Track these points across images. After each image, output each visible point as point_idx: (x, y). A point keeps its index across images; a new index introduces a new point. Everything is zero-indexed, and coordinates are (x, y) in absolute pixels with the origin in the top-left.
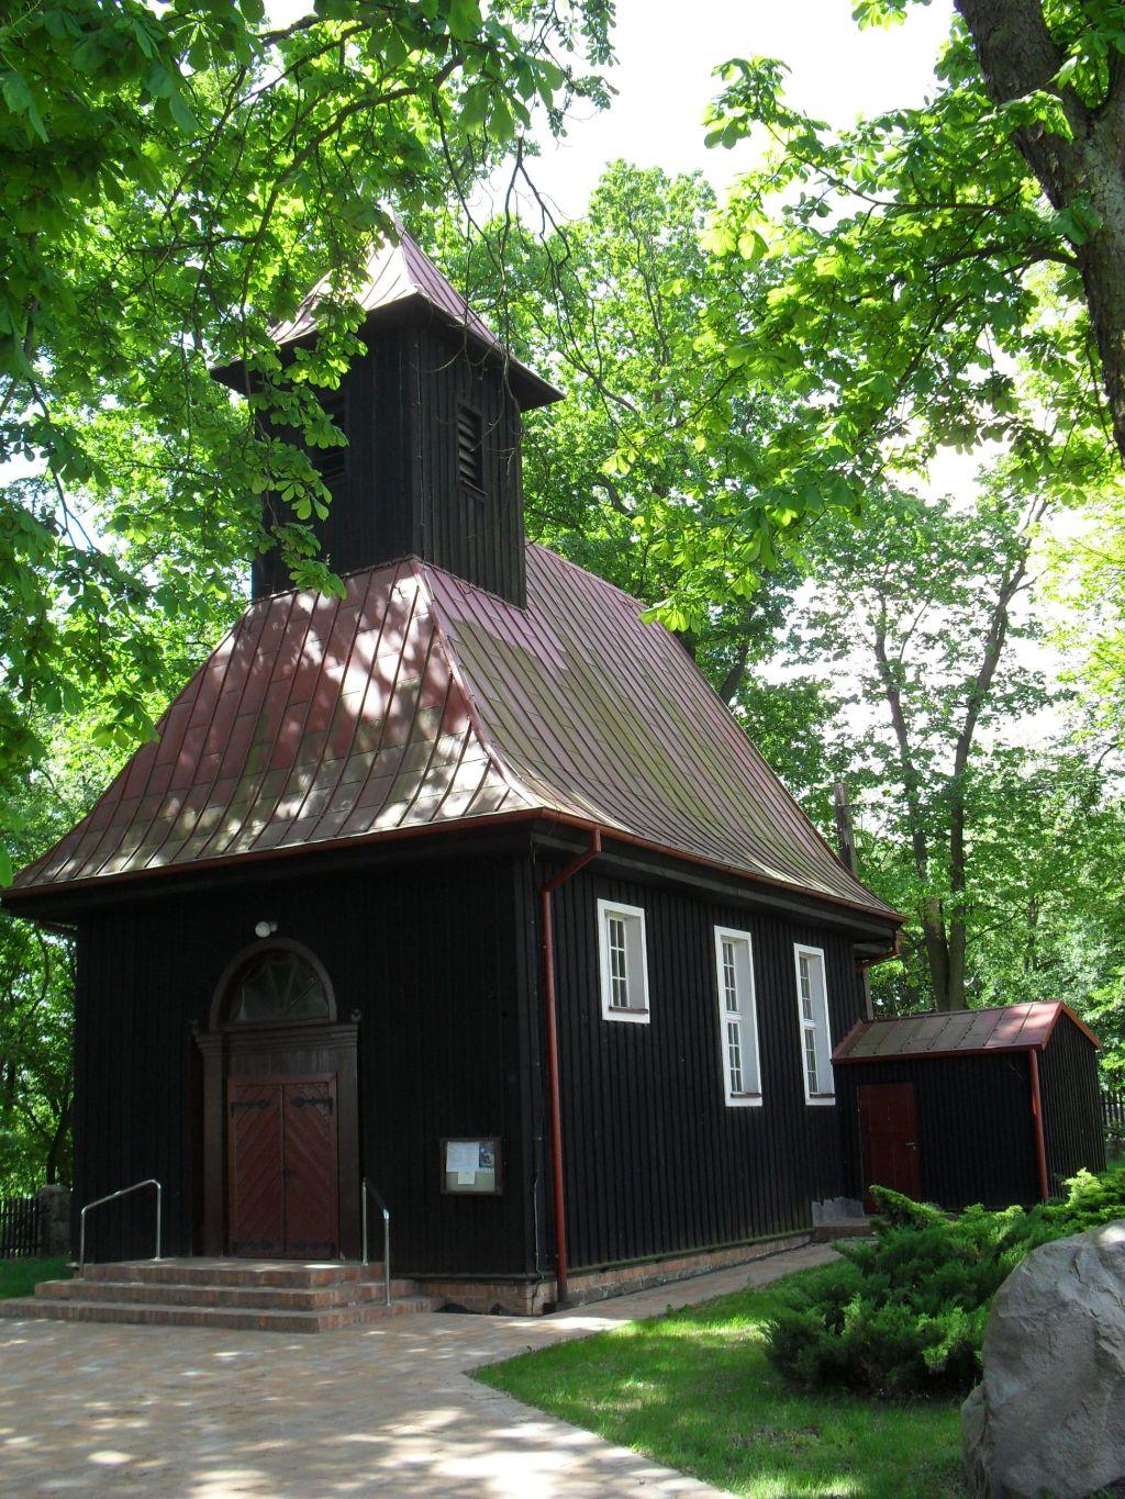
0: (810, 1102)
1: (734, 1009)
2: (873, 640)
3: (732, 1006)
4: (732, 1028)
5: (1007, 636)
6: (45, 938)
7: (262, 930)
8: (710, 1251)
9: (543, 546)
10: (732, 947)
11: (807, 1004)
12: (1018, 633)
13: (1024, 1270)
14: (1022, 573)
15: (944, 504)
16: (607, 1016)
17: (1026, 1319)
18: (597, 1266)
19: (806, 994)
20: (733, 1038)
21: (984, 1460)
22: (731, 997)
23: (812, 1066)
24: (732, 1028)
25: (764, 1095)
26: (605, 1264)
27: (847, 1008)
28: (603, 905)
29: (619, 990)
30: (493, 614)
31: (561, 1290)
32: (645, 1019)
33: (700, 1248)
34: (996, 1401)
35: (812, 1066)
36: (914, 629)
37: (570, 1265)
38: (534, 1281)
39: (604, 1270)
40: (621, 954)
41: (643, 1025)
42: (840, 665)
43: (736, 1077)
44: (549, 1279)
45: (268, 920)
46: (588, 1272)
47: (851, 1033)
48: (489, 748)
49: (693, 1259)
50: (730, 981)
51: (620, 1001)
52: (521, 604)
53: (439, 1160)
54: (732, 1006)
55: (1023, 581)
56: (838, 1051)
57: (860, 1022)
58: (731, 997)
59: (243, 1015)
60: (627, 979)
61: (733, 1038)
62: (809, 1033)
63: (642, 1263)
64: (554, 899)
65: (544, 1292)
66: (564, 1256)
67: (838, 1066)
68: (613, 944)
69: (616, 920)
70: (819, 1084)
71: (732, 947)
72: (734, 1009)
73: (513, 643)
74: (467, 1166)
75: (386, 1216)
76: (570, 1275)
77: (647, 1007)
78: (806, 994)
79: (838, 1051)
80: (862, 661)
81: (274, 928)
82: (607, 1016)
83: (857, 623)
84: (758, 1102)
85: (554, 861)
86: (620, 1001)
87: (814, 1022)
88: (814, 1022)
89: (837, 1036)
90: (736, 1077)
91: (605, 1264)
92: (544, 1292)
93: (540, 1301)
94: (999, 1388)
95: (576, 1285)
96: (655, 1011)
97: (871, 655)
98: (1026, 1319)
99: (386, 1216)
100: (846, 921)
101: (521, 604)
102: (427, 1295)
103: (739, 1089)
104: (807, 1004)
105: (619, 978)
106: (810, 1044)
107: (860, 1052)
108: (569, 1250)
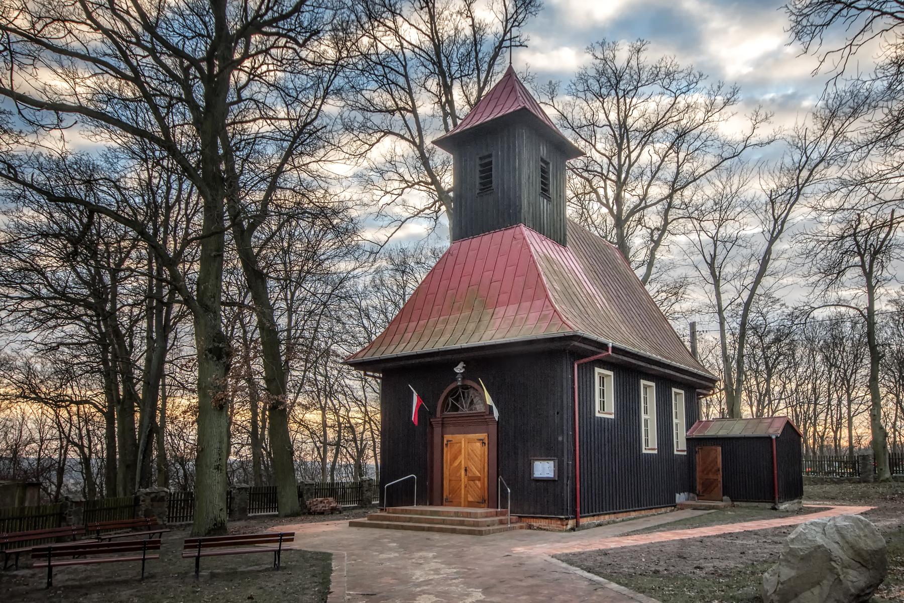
6: (230, 121)
10: (648, 392)
16: (597, 415)
24: (646, 421)
27: (692, 416)
30: (552, 248)
31: (577, 523)
44: (572, 518)
47: (694, 426)
52: (564, 246)
54: (646, 413)
63: (609, 514)
67: (688, 440)
69: (493, 159)
70: (680, 446)
71: (648, 392)
74: (544, 469)
76: (581, 517)
82: (597, 415)
85: (577, 355)
87: (679, 421)
88: (679, 421)
92: (571, 523)
93: (569, 527)
95: (584, 521)
96: (616, 413)
100: (695, 380)
101: (564, 246)
107: (696, 434)
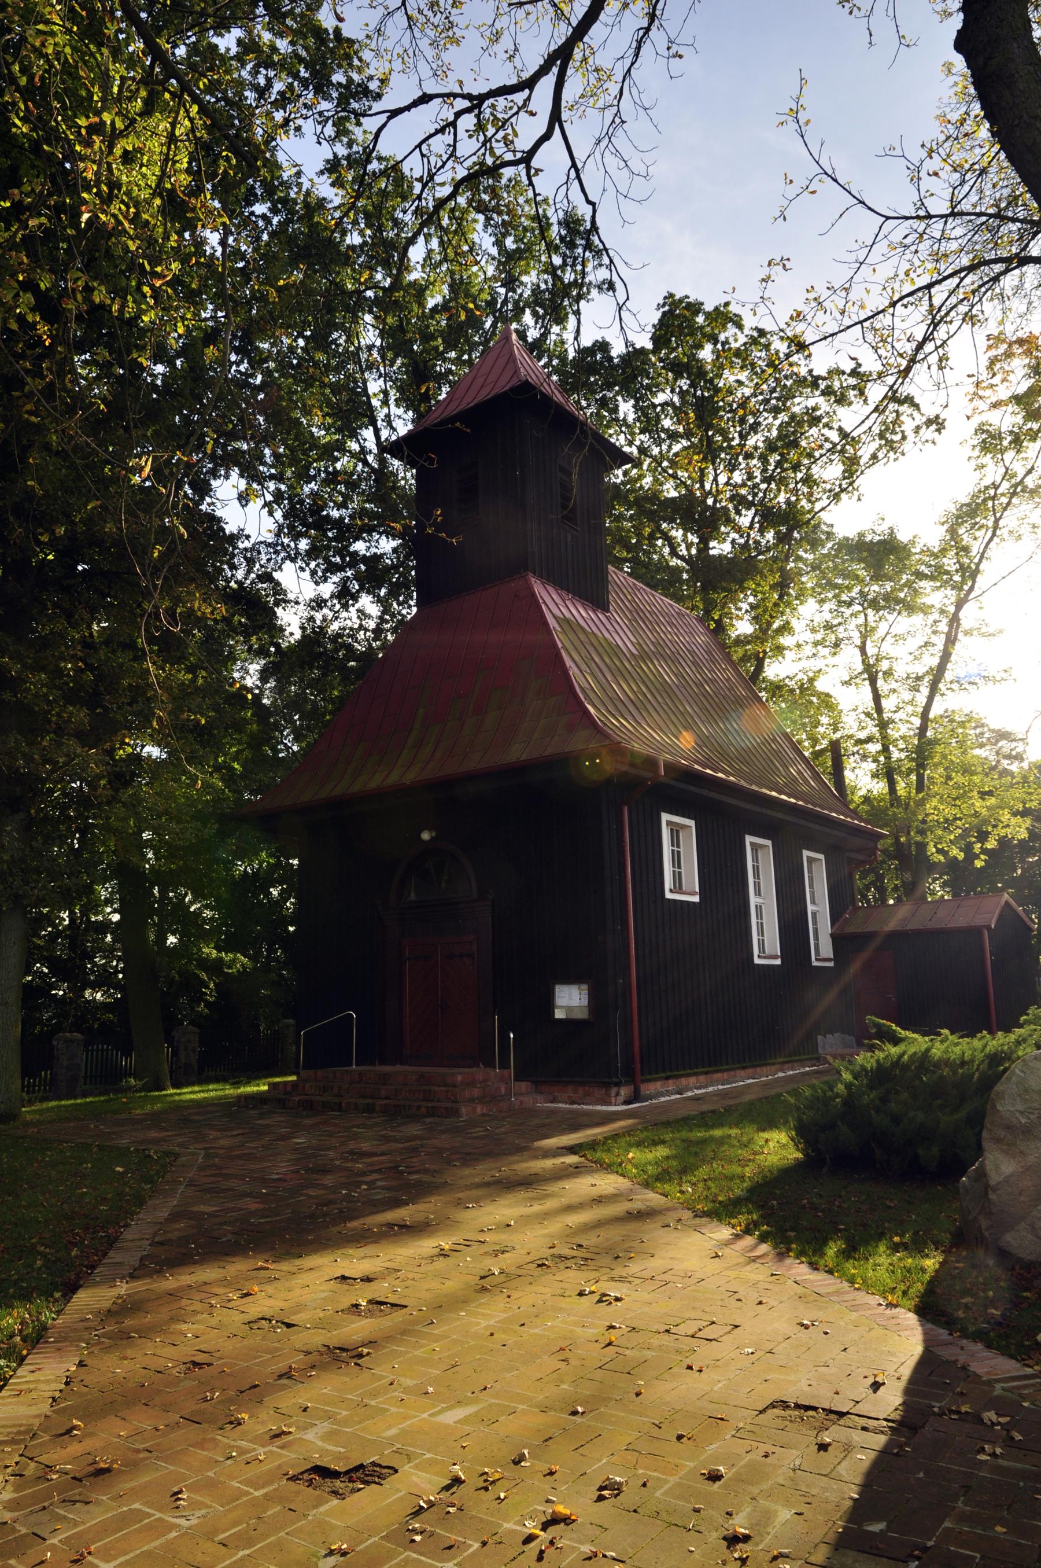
0: (815, 963)
1: (760, 895)
2: (858, 642)
3: (758, 893)
4: (759, 908)
5: (960, 636)
7: (426, 836)
8: (744, 1068)
9: (620, 576)
11: (812, 894)
12: (966, 633)
13: (1017, 1071)
14: (972, 589)
15: (913, 542)
17: (1021, 1113)
18: (663, 1075)
19: (811, 886)
20: (760, 915)
21: (983, 1227)
22: (757, 886)
23: (816, 938)
24: (759, 908)
25: (782, 957)
26: (669, 1073)
28: (665, 817)
29: (677, 878)
32: (696, 899)
33: (737, 1066)
34: (994, 1178)
35: (816, 938)
36: (888, 633)
37: (642, 1075)
38: (618, 1084)
39: (667, 1078)
40: (679, 852)
41: (694, 903)
42: (835, 660)
43: (761, 943)
44: (627, 1084)
45: (430, 830)
46: (656, 1080)
48: (668, 1137)
49: (732, 1073)
50: (756, 875)
51: (678, 888)
53: (568, 1023)
54: (758, 893)
55: (973, 595)
56: (835, 927)
57: (851, 908)
58: (757, 886)
59: (413, 896)
60: (683, 870)
61: (760, 915)
62: (814, 914)
63: (696, 1074)
64: (630, 812)
65: (624, 1091)
66: (638, 1066)
68: (673, 845)
72: (760, 895)
73: (600, 634)
75: (512, 1036)
76: (643, 1081)
77: (697, 890)
78: (811, 886)
79: (835, 927)
80: (850, 658)
81: (434, 834)
82: (669, 895)
83: (851, 630)
84: (778, 962)
86: (678, 888)
89: (834, 918)
90: (761, 943)
91: (669, 1073)
94: (997, 1168)
96: (702, 893)
97: (857, 652)
98: (1021, 1113)
99: (512, 1036)
102: (541, 1093)
103: (764, 952)
104: (812, 894)
105: (676, 849)
106: (815, 922)
107: (851, 929)
108: (642, 1062)
